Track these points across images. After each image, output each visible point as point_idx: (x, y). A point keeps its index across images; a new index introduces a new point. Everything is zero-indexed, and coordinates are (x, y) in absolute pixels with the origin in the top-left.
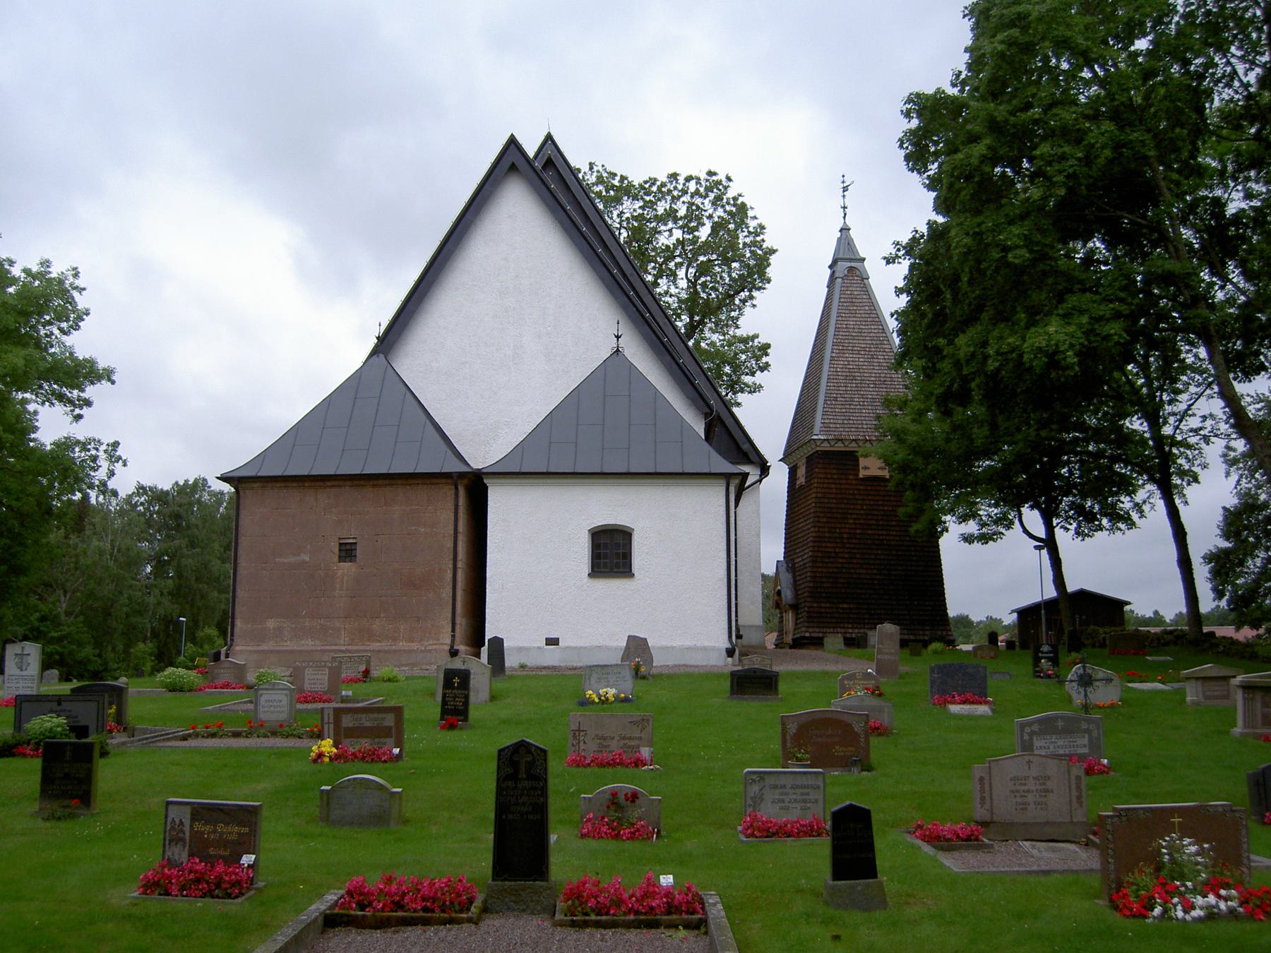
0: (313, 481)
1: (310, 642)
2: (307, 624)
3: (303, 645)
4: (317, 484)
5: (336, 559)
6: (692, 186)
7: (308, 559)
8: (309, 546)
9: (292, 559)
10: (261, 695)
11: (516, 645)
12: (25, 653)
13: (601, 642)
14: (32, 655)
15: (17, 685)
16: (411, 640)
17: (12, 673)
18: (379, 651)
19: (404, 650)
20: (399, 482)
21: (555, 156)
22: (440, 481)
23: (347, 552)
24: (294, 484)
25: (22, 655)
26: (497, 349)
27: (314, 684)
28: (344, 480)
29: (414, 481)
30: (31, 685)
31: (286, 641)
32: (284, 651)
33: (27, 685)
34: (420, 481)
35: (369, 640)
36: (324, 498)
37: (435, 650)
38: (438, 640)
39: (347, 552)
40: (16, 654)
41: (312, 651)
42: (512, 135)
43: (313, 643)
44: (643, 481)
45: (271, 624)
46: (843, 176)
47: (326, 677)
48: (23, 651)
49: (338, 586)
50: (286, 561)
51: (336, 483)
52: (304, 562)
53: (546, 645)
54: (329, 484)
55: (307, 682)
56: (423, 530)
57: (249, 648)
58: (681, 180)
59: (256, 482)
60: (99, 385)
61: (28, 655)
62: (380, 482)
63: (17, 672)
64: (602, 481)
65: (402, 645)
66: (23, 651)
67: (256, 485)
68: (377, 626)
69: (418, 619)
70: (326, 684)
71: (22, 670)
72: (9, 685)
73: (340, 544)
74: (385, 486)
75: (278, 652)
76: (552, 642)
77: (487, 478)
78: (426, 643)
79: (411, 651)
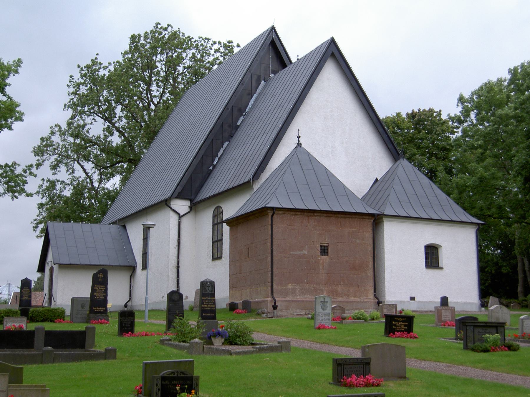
0: (309, 212)
1: (309, 296)
2: (307, 287)
3: (306, 298)
4: (310, 214)
5: (320, 254)
6: (216, 47)
7: (306, 253)
8: (306, 246)
9: (298, 253)
10: (524, 321)
11: (398, 300)
12: (325, 301)
13: (432, 300)
14: (329, 302)
15: (322, 318)
16: (355, 296)
17: (319, 311)
18: (343, 302)
19: (355, 302)
20: (348, 216)
21: (275, 39)
22: (365, 217)
23: (324, 250)
24: (299, 213)
25: (324, 302)
26: (324, 147)
27: (446, 317)
28: (324, 213)
29: (354, 216)
30: (329, 318)
31: (297, 296)
32: (299, 301)
33: (327, 318)
34: (357, 217)
35: (336, 296)
36: (312, 221)
37: (368, 302)
38: (367, 297)
39: (324, 250)
40: (321, 302)
41: (312, 301)
42: (273, 28)
43: (310, 297)
44: (463, 225)
45: (290, 286)
46: (298, 56)
47: (450, 314)
48: (324, 300)
49: (321, 268)
50: (295, 253)
51: (319, 214)
52: (304, 254)
53: (410, 300)
54: (316, 214)
55: (443, 316)
56: (358, 241)
57: (281, 299)
58: (211, 42)
59: (281, 211)
60: (8, 130)
61: (327, 302)
62: (340, 215)
63: (321, 311)
64: (437, 223)
65: (351, 299)
66: (324, 300)
67: (281, 212)
68: (340, 289)
69: (358, 286)
70: (450, 318)
71: (324, 310)
72: (319, 318)
73: (321, 246)
74: (341, 217)
75: (296, 301)
76: (413, 299)
77: (384, 217)
78: (362, 298)
79: (357, 302)
